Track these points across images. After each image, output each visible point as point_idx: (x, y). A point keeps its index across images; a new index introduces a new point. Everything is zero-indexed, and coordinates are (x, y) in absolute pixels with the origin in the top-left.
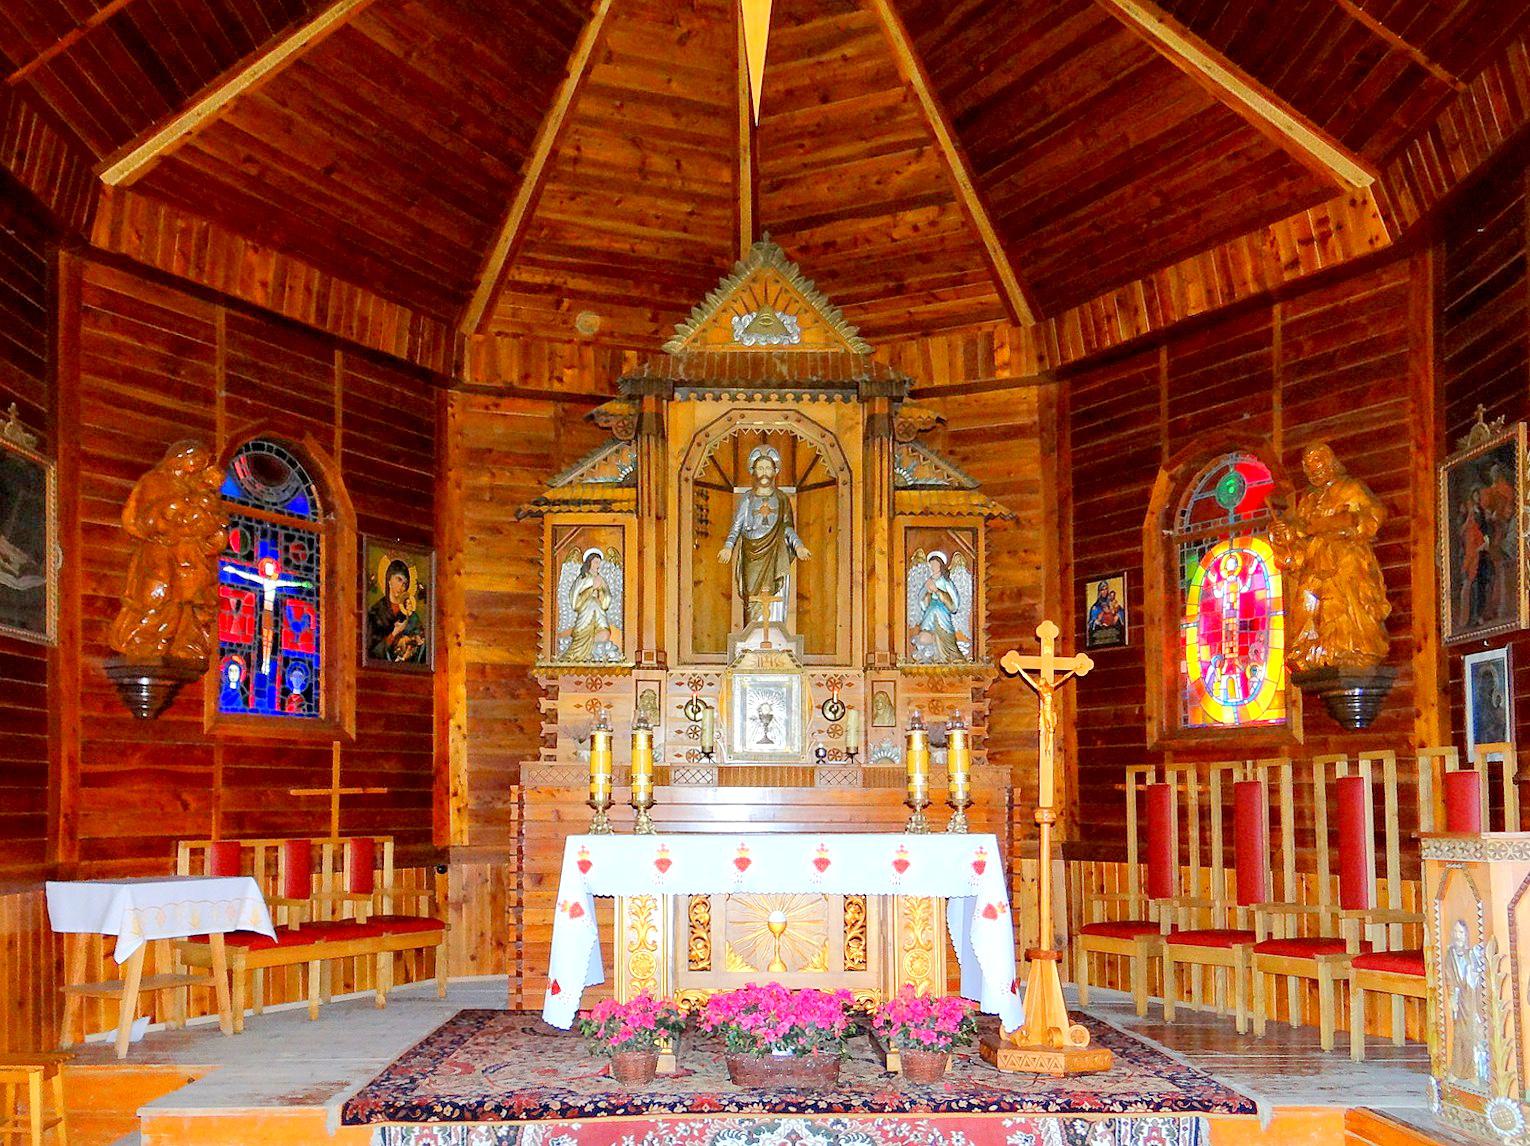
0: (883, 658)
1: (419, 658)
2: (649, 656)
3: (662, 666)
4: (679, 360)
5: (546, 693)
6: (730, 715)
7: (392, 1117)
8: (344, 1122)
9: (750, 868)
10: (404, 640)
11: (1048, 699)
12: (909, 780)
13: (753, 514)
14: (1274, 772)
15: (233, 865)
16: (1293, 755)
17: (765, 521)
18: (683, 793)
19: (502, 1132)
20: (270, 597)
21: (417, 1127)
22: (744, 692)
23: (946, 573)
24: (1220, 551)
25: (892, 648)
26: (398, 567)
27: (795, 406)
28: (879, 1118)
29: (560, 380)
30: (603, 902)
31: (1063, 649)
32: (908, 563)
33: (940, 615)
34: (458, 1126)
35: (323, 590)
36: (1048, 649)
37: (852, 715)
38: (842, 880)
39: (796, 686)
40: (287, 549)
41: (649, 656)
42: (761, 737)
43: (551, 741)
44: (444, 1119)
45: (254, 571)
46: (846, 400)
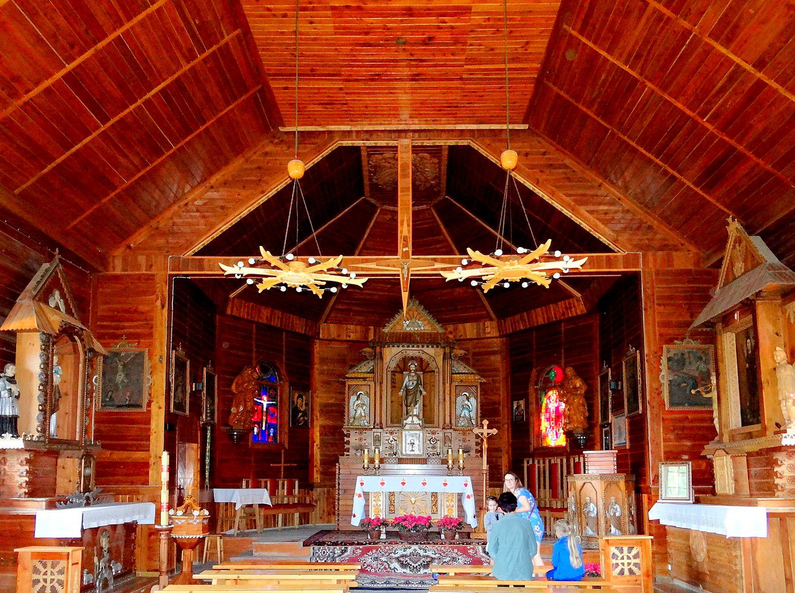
0: (448, 425)
1: (306, 423)
2: (377, 425)
3: (381, 428)
4: (387, 335)
5: (346, 436)
6: (402, 444)
7: (316, 545)
8: (304, 546)
9: (405, 485)
10: (302, 418)
11: (485, 440)
12: (448, 462)
13: (409, 381)
14: (562, 461)
15: (257, 486)
16: (566, 456)
17: (413, 383)
18: (388, 466)
19: (343, 549)
20: (265, 406)
21: (322, 547)
22: (406, 436)
23: (468, 399)
24: (550, 393)
25: (451, 423)
26: (300, 396)
27: (422, 349)
28: (437, 546)
29: (349, 336)
30: (366, 495)
31: (489, 427)
32: (456, 396)
33: (466, 412)
34: (332, 547)
35: (279, 404)
36: (485, 427)
37: (438, 442)
38: (430, 489)
39: (421, 434)
40: (269, 392)
41: (377, 425)
42: (411, 449)
43: (348, 450)
44: (328, 545)
45: (261, 399)
46: (437, 347)
